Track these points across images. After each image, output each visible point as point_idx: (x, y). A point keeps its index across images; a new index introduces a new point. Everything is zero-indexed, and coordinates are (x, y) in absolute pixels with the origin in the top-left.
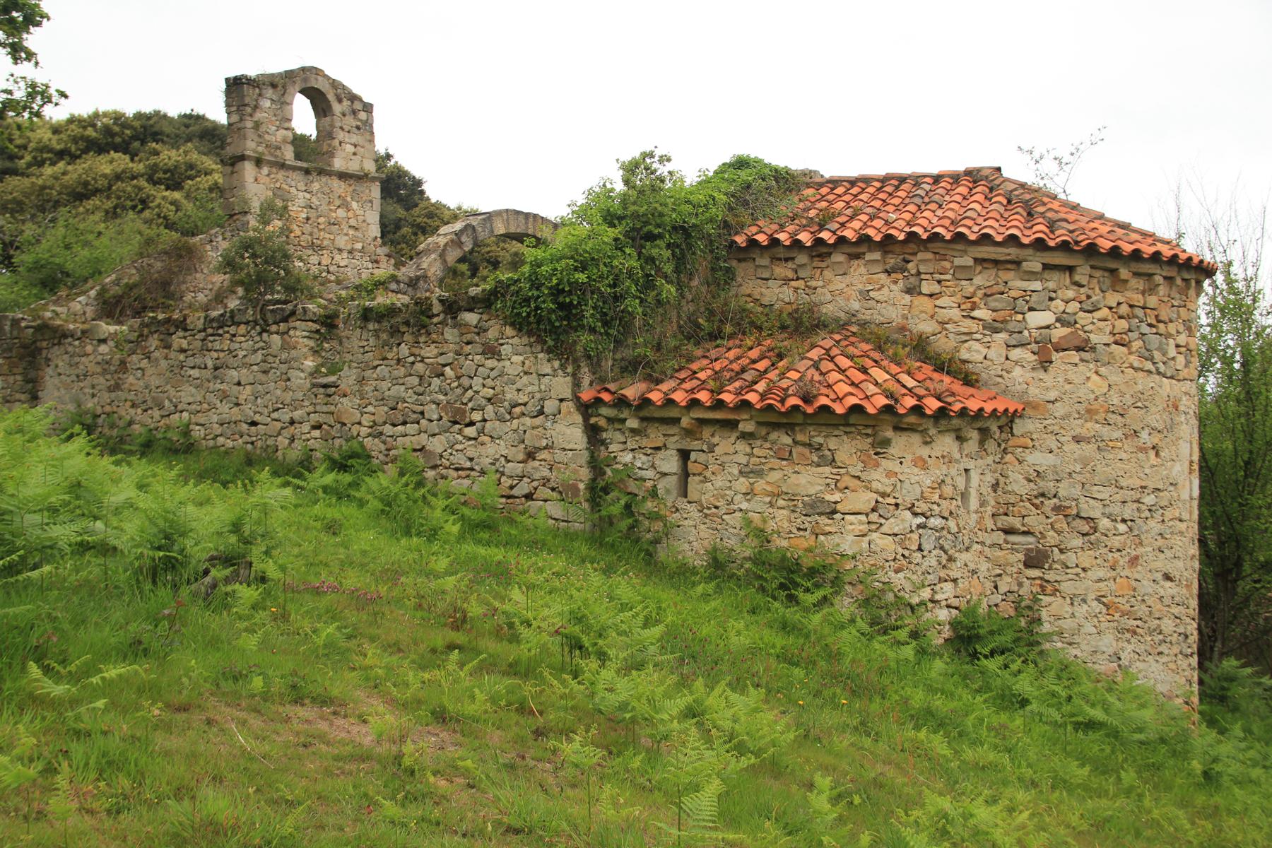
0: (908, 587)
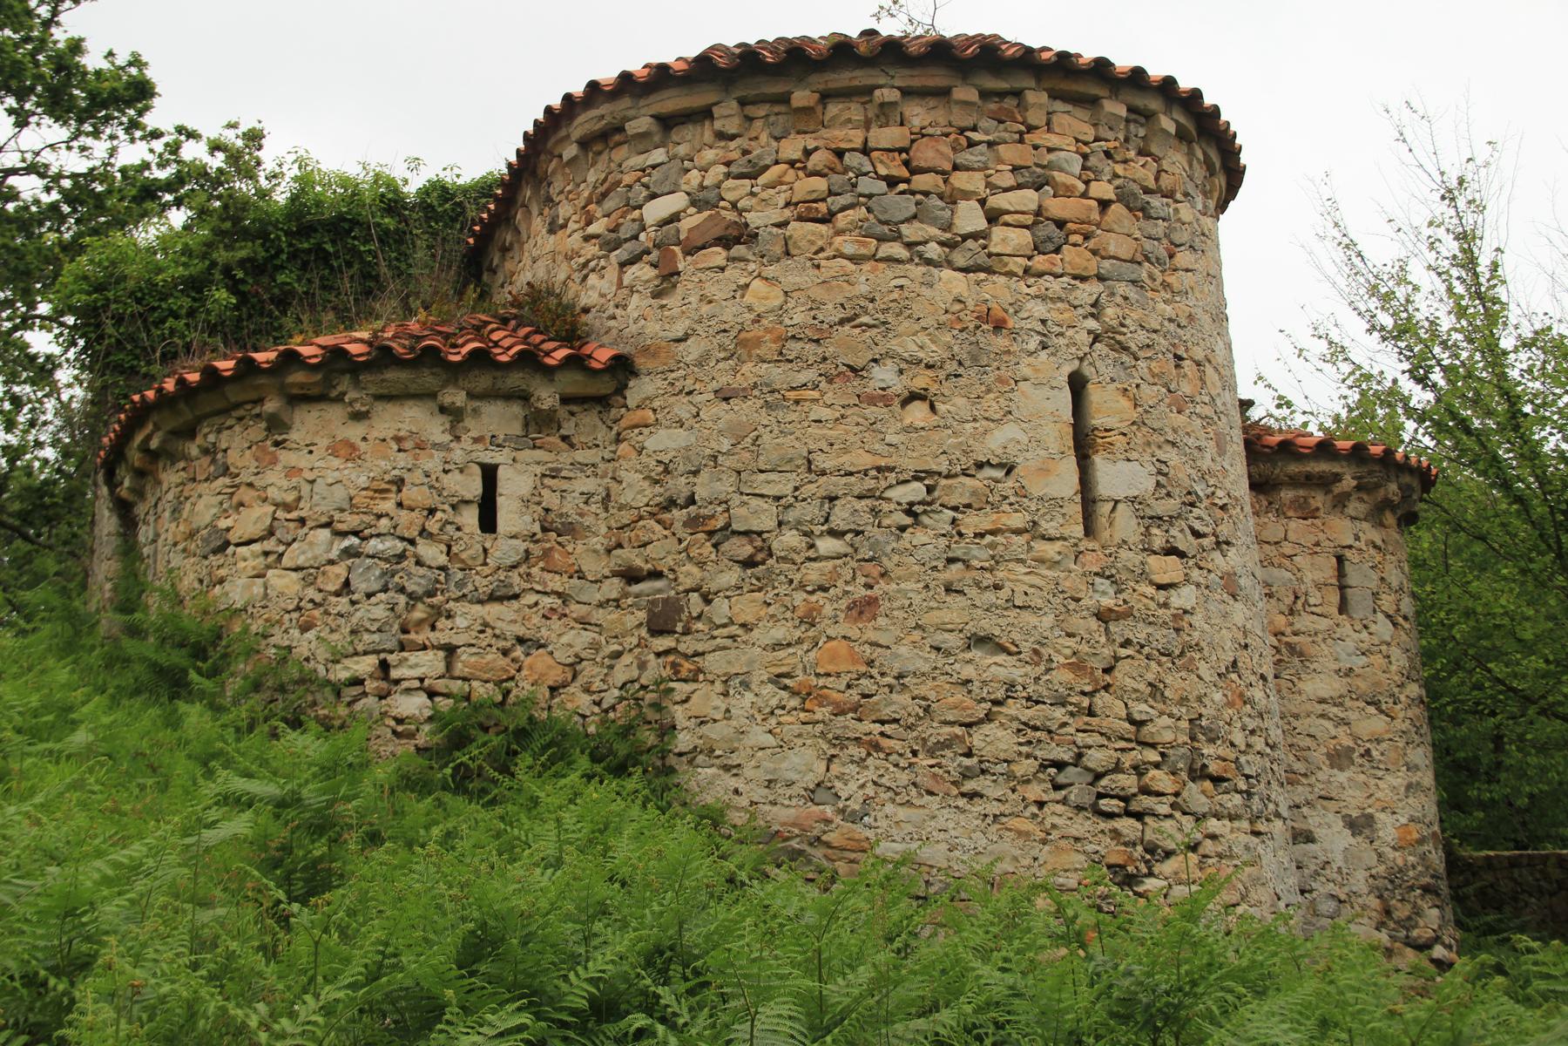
0: (322, 654)
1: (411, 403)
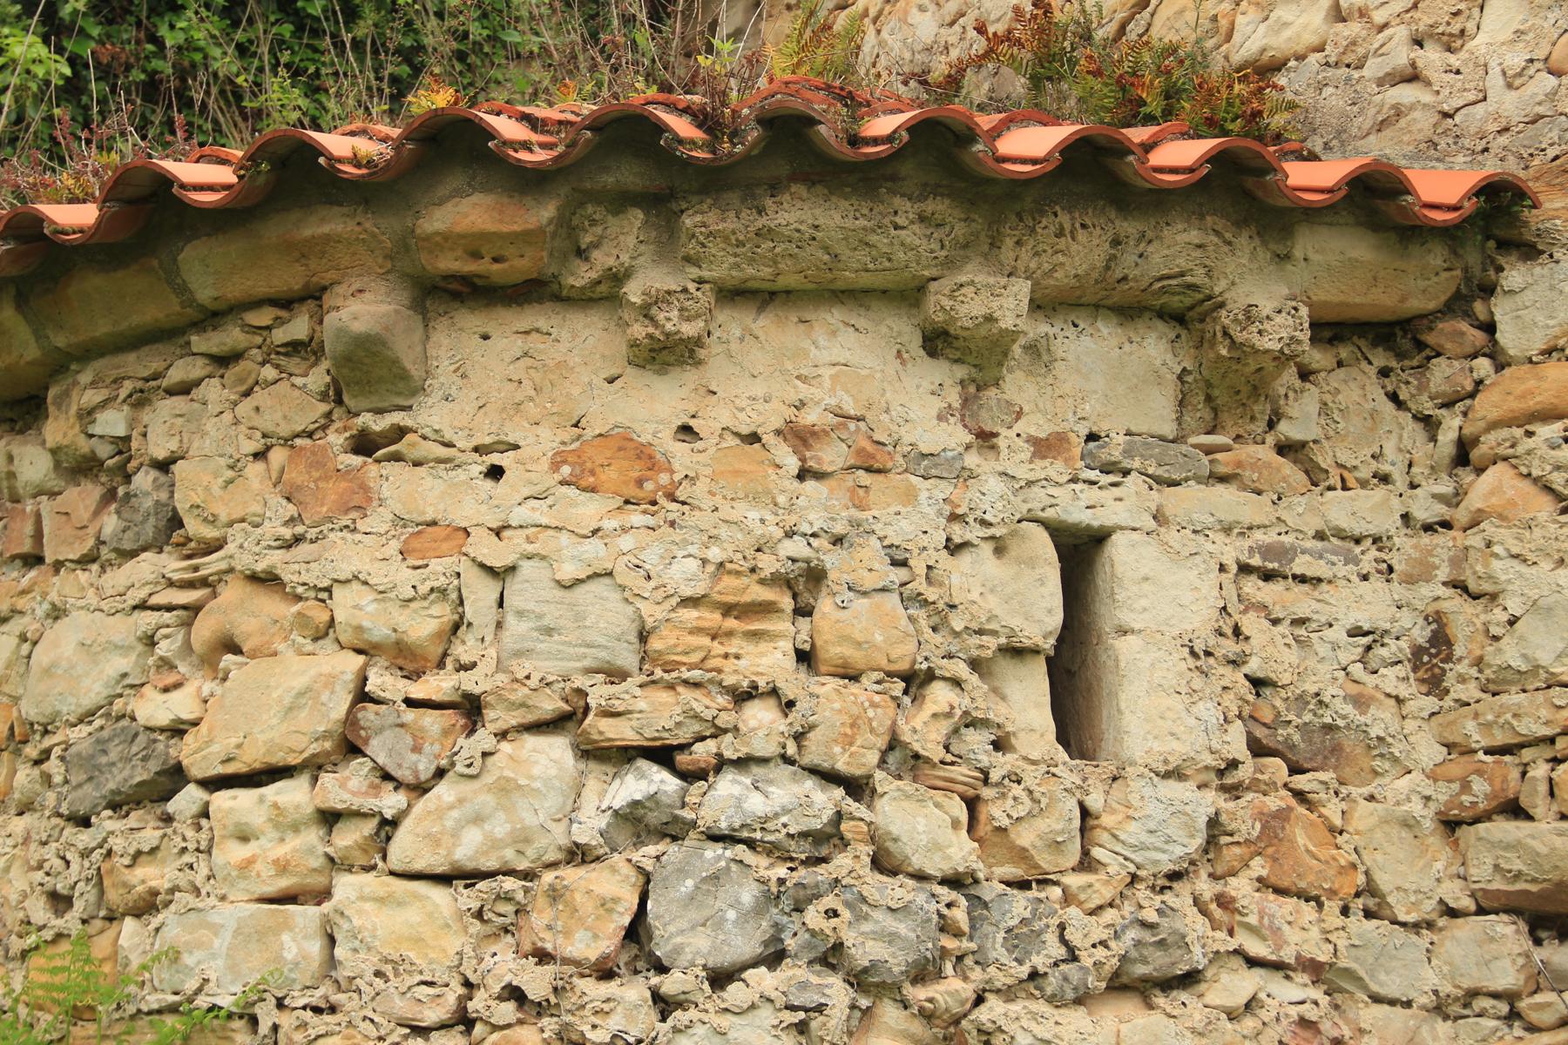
1: (835, 316)
